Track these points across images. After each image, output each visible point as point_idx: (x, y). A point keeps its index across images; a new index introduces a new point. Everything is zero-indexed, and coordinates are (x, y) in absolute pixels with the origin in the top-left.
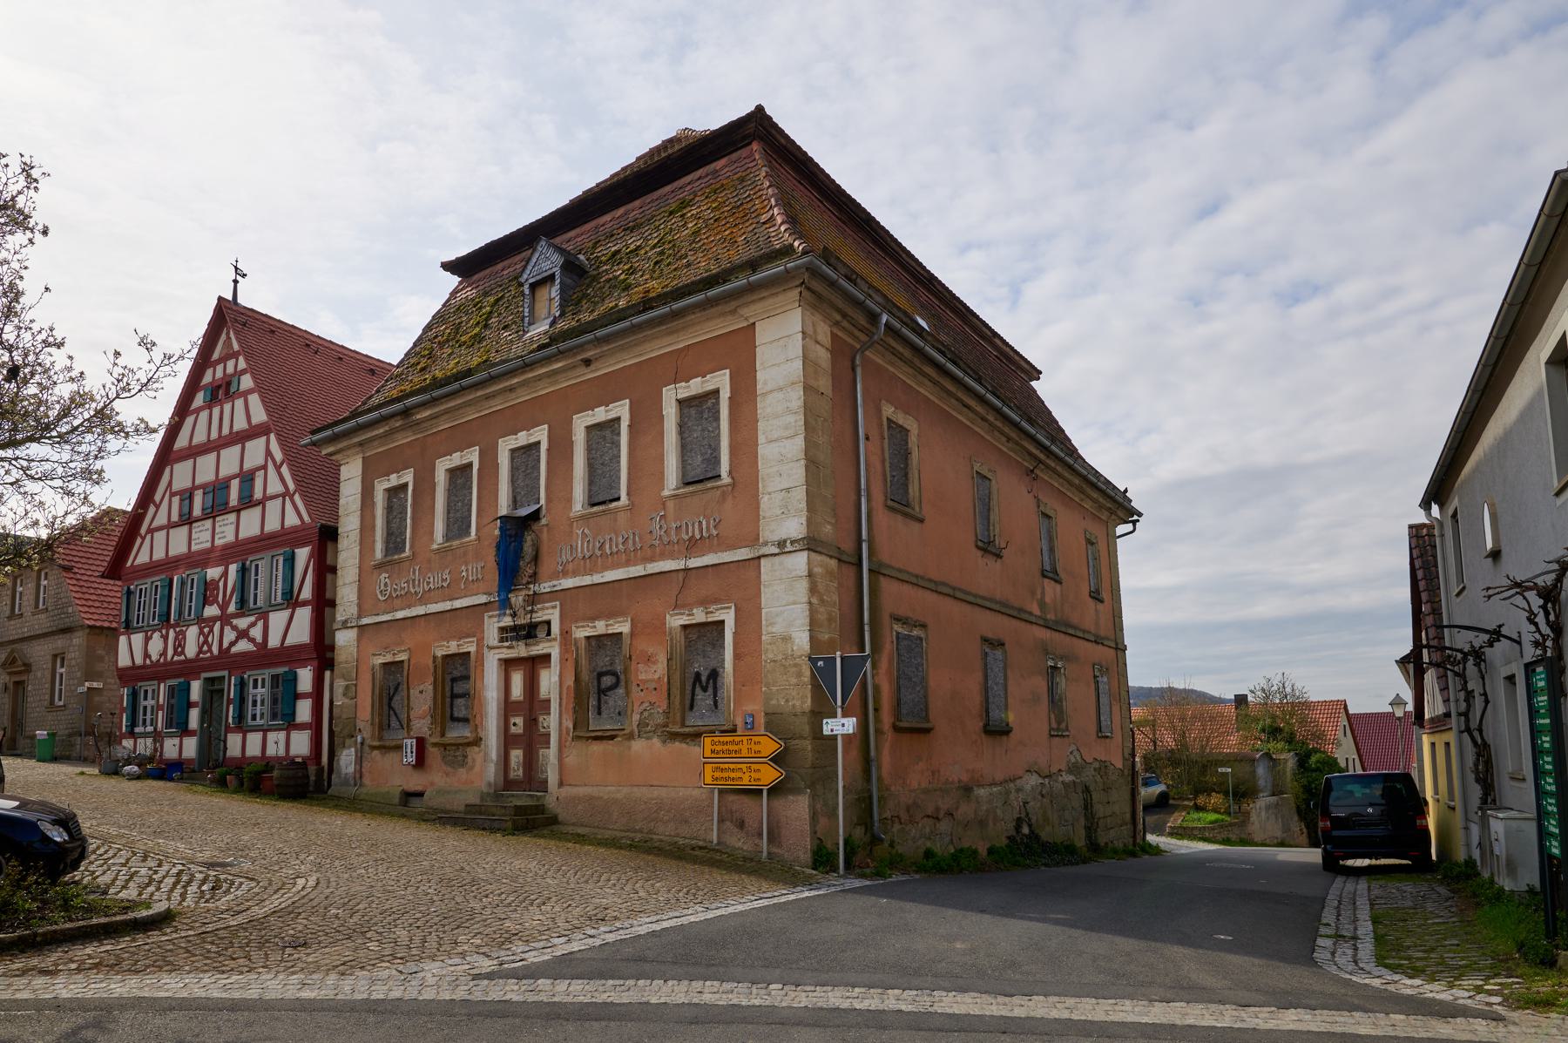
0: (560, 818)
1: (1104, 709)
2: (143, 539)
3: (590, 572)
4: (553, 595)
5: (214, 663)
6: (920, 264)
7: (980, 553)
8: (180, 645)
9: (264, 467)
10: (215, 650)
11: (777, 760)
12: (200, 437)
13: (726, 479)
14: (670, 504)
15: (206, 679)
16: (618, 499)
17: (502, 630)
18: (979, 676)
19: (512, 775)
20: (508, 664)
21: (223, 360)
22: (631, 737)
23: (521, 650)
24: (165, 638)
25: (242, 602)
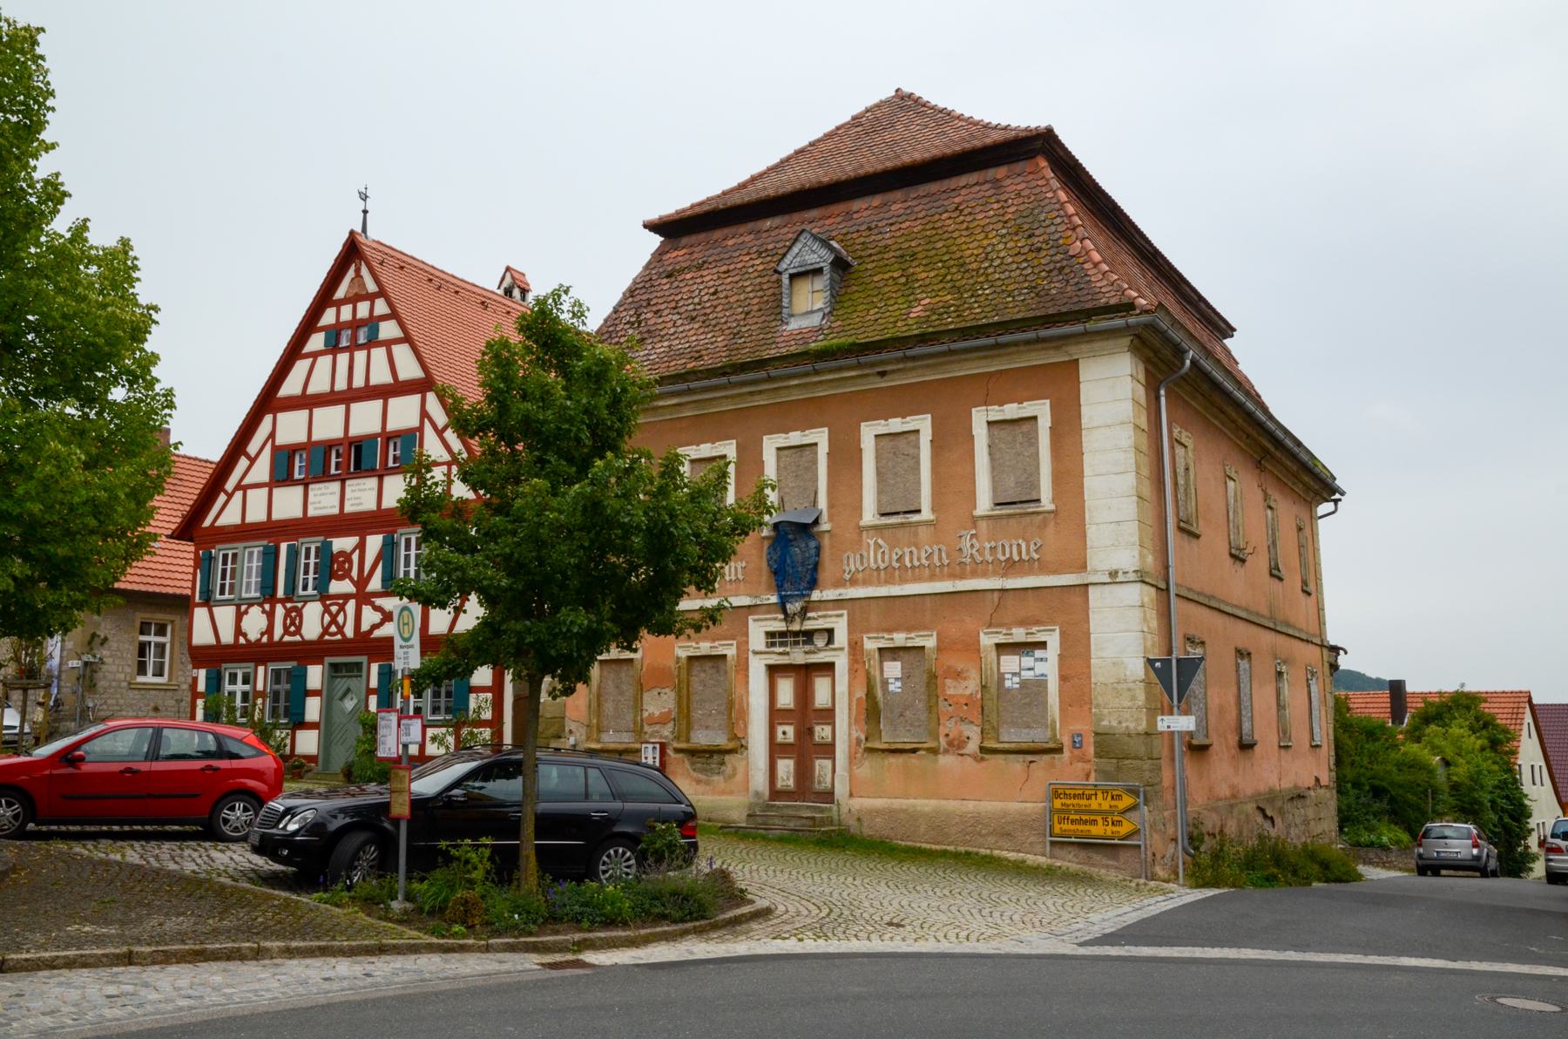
2: (230, 496)
3: (889, 581)
4: (839, 603)
5: (345, 647)
6: (1148, 242)
7: (1229, 561)
8: (294, 620)
9: (421, 429)
10: (349, 632)
12: (319, 385)
13: (1047, 503)
15: (332, 665)
18: (1234, 689)
19: (780, 784)
20: (773, 670)
21: (353, 300)
22: (934, 751)
23: (798, 656)
24: (271, 616)
25: (389, 577)
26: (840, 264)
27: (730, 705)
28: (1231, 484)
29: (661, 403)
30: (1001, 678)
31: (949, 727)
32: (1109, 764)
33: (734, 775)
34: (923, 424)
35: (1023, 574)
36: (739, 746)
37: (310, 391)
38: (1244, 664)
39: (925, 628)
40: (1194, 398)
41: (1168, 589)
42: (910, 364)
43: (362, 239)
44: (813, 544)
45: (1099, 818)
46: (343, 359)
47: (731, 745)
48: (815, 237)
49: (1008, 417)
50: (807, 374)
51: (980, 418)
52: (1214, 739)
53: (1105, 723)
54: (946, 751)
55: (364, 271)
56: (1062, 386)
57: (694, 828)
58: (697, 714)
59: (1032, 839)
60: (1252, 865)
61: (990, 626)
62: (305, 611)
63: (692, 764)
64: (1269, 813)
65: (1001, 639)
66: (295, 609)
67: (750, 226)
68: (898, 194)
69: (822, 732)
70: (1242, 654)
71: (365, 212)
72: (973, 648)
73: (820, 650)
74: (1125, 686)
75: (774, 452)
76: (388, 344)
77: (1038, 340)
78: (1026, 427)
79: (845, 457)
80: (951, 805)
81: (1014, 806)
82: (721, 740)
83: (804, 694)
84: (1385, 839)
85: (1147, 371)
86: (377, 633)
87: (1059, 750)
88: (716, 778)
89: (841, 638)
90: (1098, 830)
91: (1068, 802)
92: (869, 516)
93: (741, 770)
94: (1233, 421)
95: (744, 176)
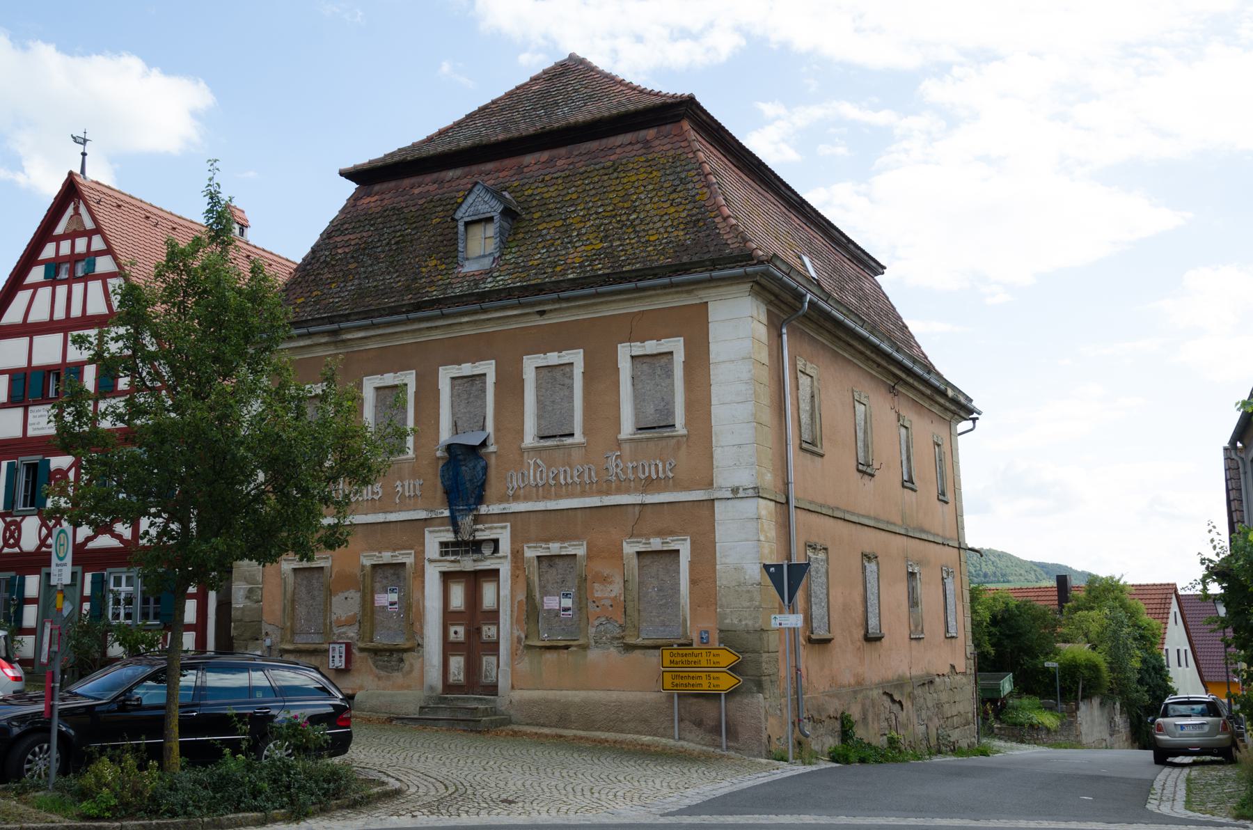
0: (514, 719)
1: (951, 607)
3: (546, 497)
4: (503, 516)
7: (859, 475)
11: (734, 669)
12: (39, 314)
13: (680, 429)
14: (626, 447)
16: (572, 435)
17: (444, 545)
18: (861, 588)
19: (451, 679)
20: (447, 577)
21: (72, 236)
23: (468, 563)
26: (508, 213)
28: (860, 409)
29: (349, 336)
33: (411, 671)
34: (576, 357)
35: (660, 490)
37: (31, 319)
38: (871, 567)
39: (577, 538)
40: (820, 334)
41: (787, 502)
42: (564, 305)
43: (80, 180)
46: (62, 290)
47: (408, 645)
48: (487, 190)
49: (648, 352)
50: (475, 312)
51: (625, 352)
52: (837, 633)
53: (728, 621)
55: (82, 210)
57: (348, 720)
61: (631, 536)
62: (24, 525)
63: (374, 663)
64: (897, 698)
65: (641, 548)
66: (14, 523)
67: (435, 176)
68: (563, 151)
69: (488, 631)
70: (867, 557)
71: (84, 154)
72: (618, 554)
73: (486, 558)
74: (744, 589)
75: (448, 381)
76: (104, 277)
77: (672, 285)
78: (664, 360)
79: (510, 386)
80: (551, 694)
82: (400, 641)
83: (473, 597)
86: (91, 545)
88: (396, 674)
89: (505, 547)
92: (529, 439)
93: (417, 666)
95: (433, 130)
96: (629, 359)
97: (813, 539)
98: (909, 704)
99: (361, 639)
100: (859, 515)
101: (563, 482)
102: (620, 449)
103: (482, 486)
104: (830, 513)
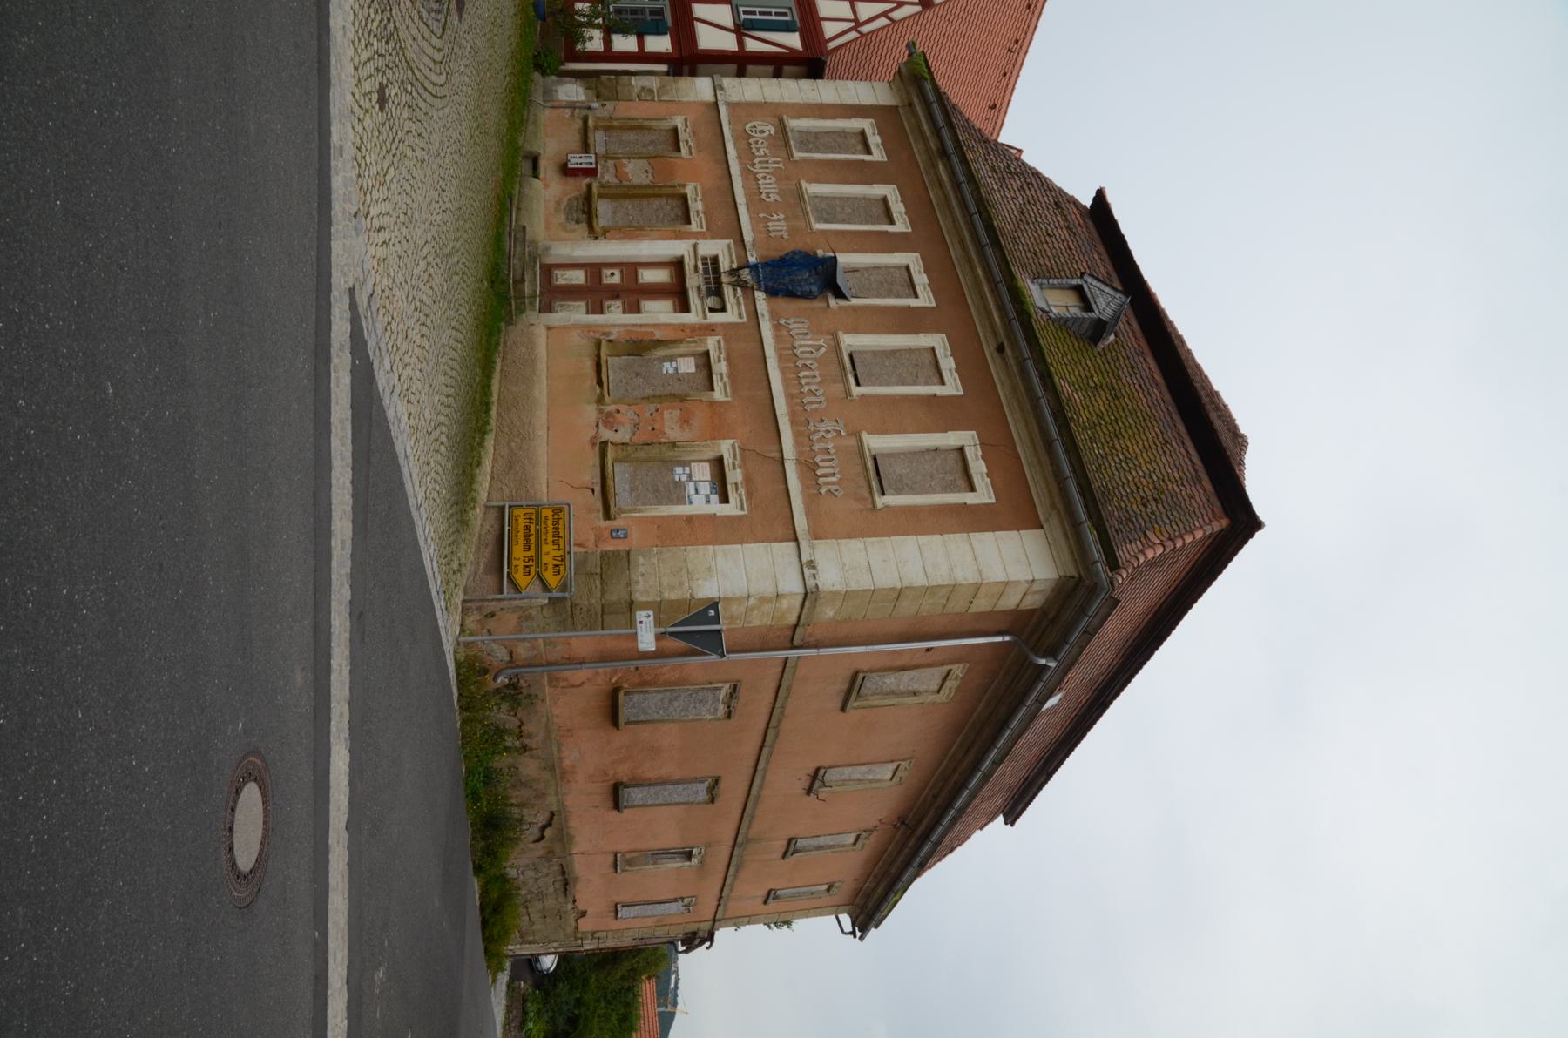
3: (780, 357)
4: (754, 315)
7: (811, 771)
13: (881, 501)
18: (677, 776)
19: (558, 272)
20: (678, 265)
22: (600, 400)
23: (694, 281)
26: (1099, 329)
27: (641, 228)
30: (684, 464)
31: (627, 415)
32: (594, 565)
36: (594, 233)
38: (701, 792)
39: (734, 392)
41: (794, 647)
44: (814, 288)
45: (532, 553)
47: (597, 229)
52: (621, 738)
53: (641, 560)
54: (601, 411)
56: (1016, 512)
58: (628, 204)
59: (507, 491)
60: (487, 716)
64: (548, 832)
72: (718, 433)
79: (910, 321)
80: (542, 415)
81: (543, 477)
82: (601, 222)
83: (655, 292)
84: (531, 1025)
85: (1033, 611)
87: (608, 516)
90: (519, 552)
91: (550, 523)
92: (849, 341)
94: (955, 769)
96: (960, 443)
97: (743, 692)
98: (541, 852)
99: (602, 186)
100: (765, 770)
101: (802, 374)
102: (848, 434)
103: (791, 294)
104: (773, 723)
